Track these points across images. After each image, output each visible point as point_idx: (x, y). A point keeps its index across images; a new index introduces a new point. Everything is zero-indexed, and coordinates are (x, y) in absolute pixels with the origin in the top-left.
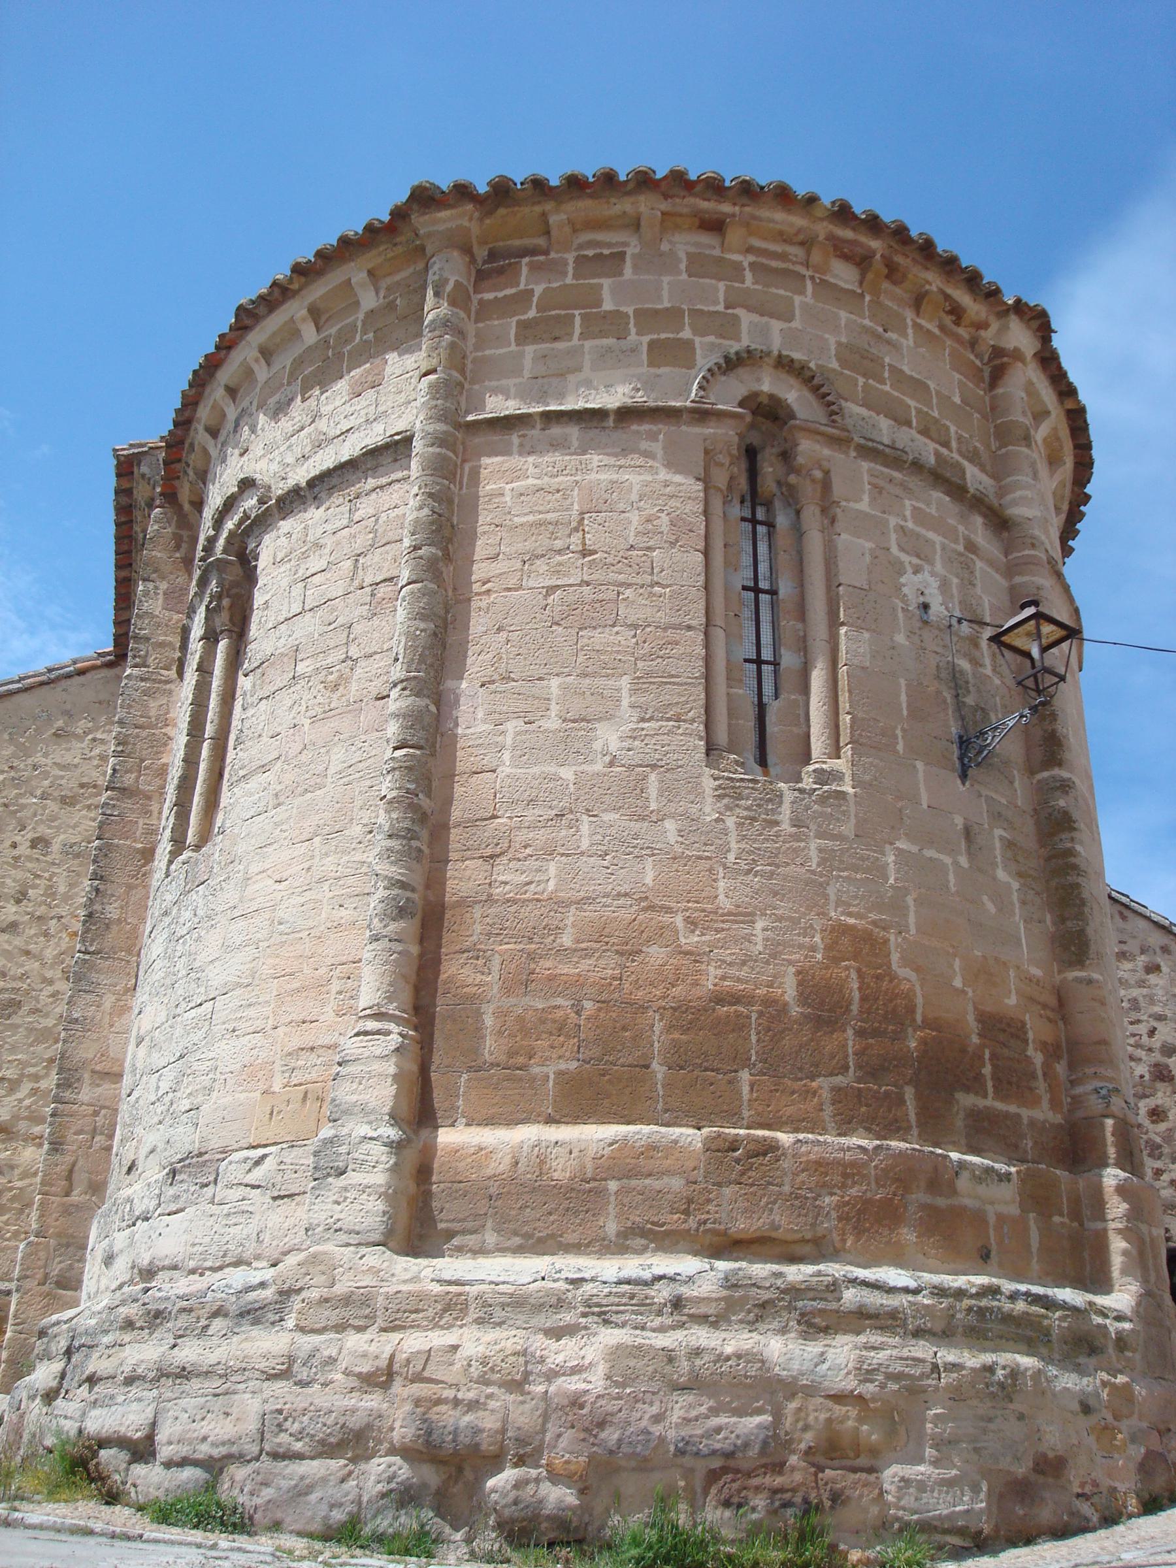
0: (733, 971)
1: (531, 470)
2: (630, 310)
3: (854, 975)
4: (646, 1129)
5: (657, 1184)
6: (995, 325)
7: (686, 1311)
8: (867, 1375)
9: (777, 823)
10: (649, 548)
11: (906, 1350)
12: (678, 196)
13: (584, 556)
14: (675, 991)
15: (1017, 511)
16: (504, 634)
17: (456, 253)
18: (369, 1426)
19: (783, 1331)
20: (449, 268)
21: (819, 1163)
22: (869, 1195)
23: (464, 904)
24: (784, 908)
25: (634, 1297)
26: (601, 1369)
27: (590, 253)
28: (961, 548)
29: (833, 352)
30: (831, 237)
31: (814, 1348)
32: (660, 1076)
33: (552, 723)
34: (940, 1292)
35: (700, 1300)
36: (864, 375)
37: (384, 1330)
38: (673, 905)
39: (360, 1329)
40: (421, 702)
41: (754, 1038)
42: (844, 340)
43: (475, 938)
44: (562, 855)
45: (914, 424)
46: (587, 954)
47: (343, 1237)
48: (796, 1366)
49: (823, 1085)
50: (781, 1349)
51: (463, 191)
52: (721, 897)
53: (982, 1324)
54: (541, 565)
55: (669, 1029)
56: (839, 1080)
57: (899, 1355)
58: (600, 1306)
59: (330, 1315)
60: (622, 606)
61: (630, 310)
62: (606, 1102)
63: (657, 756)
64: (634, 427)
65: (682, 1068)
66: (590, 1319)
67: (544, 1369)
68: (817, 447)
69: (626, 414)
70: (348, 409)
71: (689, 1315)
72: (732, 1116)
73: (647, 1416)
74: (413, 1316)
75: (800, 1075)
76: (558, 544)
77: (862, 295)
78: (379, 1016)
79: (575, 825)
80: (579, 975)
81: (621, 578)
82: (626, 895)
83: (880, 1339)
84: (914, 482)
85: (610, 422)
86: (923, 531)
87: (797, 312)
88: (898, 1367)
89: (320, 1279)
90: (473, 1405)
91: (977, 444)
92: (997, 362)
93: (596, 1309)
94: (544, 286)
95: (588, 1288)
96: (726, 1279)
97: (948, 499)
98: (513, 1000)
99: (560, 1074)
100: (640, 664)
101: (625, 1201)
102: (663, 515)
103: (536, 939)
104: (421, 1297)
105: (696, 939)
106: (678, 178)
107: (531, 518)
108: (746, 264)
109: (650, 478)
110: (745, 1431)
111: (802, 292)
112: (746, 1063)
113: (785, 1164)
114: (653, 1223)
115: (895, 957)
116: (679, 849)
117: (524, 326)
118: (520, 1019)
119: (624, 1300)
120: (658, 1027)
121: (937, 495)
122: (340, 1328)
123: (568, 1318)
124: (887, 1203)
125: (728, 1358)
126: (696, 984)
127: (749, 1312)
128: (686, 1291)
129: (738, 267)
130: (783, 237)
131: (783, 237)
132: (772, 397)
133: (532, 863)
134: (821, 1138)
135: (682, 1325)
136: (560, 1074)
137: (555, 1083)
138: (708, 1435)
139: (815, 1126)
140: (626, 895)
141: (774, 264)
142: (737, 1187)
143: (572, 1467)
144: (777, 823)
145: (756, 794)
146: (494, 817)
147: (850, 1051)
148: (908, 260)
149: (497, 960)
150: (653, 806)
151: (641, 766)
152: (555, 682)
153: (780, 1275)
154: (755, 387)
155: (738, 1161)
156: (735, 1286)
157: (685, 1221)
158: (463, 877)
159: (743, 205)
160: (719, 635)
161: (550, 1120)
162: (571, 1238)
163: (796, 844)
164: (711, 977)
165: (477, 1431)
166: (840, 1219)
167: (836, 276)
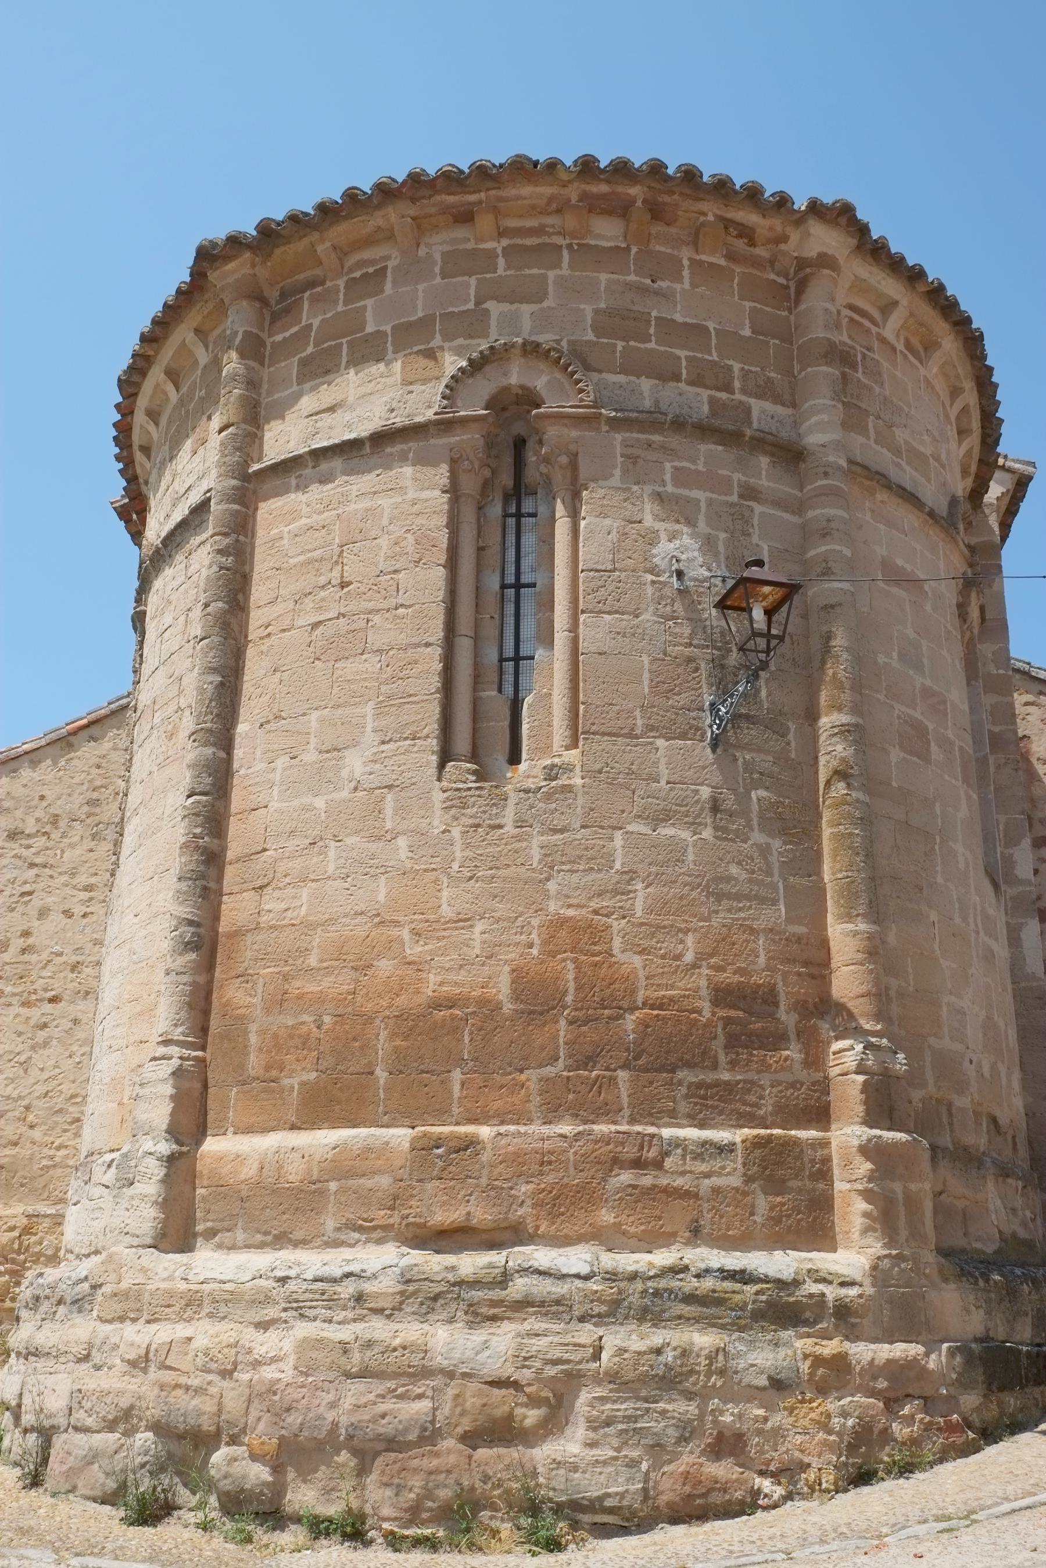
0: (452, 977)
1: (305, 510)
2: (387, 328)
3: (570, 966)
4: (363, 1132)
5: (368, 1183)
6: (794, 236)
7: (367, 1305)
8: (524, 1361)
9: (500, 827)
10: (395, 571)
11: (569, 1336)
12: (424, 197)
13: (343, 588)
14: (399, 1001)
15: (813, 439)
16: (278, 674)
17: (244, 303)
18: (132, 1407)
19: (451, 1321)
20: (239, 320)
21: (517, 1154)
22: (566, 1180)
23: (237, 934)
24: (502, 909)
25: (325, 1295)
26: (291, 1360)
27: (357, 274)
28: (734, 498)
29: (589, 322)
30: (584, 196)
31: (479, 1336)
32: (382, 1082)
33: (310, 756)
34: (612, 1276)
35: (377, 1295)
36: (623, 339)
37: (148, 1322)
38: (400, 919)
39: (134, 1320)
40: (209, 751)
41: (467, 1039)
42: (603, 306)
43: (246, 964)
44: (313, 881)
45: (684, 376)
46: (328, 971)
47: (129, 1240)
48: (457, 1355)
49: (531, 1077)
50: (447, 1340)
51: (235, 241)
52: (445, 907)
53: (656, 1302)
54: (308, 603)
55: (393, 1036)
56: (550, 1071)
57: (562, 1341)
58: (297, 1301)
59: (117, 1308)
60: (370, 633)
61: (387, 328)
62: (337, 1108)
63: (394, 777)
64: (389, 450)
65: (401, 1072)
66: (289, 1314)
67: (251, 1359)
68: (565, 431)
69: (381, 439)
70: (190, 467)
71: (370, 1309)
72: (441, 1114)
73: (324, 1403)
74: (167, 1310)
75: (509, 1069)
76: (322, 580)
77: (628, 249)
78: (167, 1043)
79: (323, 852)
80: (321, 992)
81: (371, 605)
82: (362, 913)
83: (544, 1326)
84: (674, 441)
85: (367, 449)
86: (685, 492)
87: (551, 289)
88: (557, 1354)
89: (113, 1277)
90: (199, 1391)
91: (773, 375)
92: (801, 275)
93: (295, 1305)
94: (320, 318)
95: (292, 1286)
96: (402, 1274)
97: (720, 448)
98: (271, 1019)
99: (303, 1084)
100: (383, 688)
101: (343, 1199)
102: (409, 535)
103: (290, 962)
104: (170, 1293)
105: (420, 949)
106: (416, 179)
107: (302, 558)
108: (499, 251)
109: (400, 500)
110: (408, 1416)
111: (558, 265)
112: (461, 1062)
113: (485, 1157)
114: (365, 1220)
115: (617, 943)
116: (408, 864)
117: (304, 363)
118: (275, 1036)
119: (317, 1297)
120: (382, 1037)
121: (708, 448)
122: (122, 1319)
123: (272, 1312)
124: (581, 1189)
125: (395, 1350)
126: (418, 992)
127: (422, 1304)
128: (368, 1287)
129: (491, 256)
130: (534, 210)
131: (534, 210)
132: (522, 387)
133: (290, 891)
134: (522, 1129)
135: (361, 1319)
136: (303, 1084)
137: (299, 1093)
138: (374, 1420)
139: (521, 1117)
140: (362, 913)
141: (529, 242)
142: (437, 1183)
143: (266, 1448)
144: (500, 827)
145: (481, 801)
146: (265, 850)
147: (561, 1040)
148: (675, 197)
149: (261, 981)
150: (389, 825)
151: (380, 788)
152: (314, 716)
153: (453, 1268)
154: (504, 382)
155: (440, 1157)
156: (408, 1281)
157: (391, 1216)
158: (235, 910)
159: (488, 190)
160: (464, 646)
161: (293, 1127)
162: (298, 1235)
163: (517, 845)
164: (432, 984)
165: (200, 1414)
166: (534, 1206)
167: (599, 237)
